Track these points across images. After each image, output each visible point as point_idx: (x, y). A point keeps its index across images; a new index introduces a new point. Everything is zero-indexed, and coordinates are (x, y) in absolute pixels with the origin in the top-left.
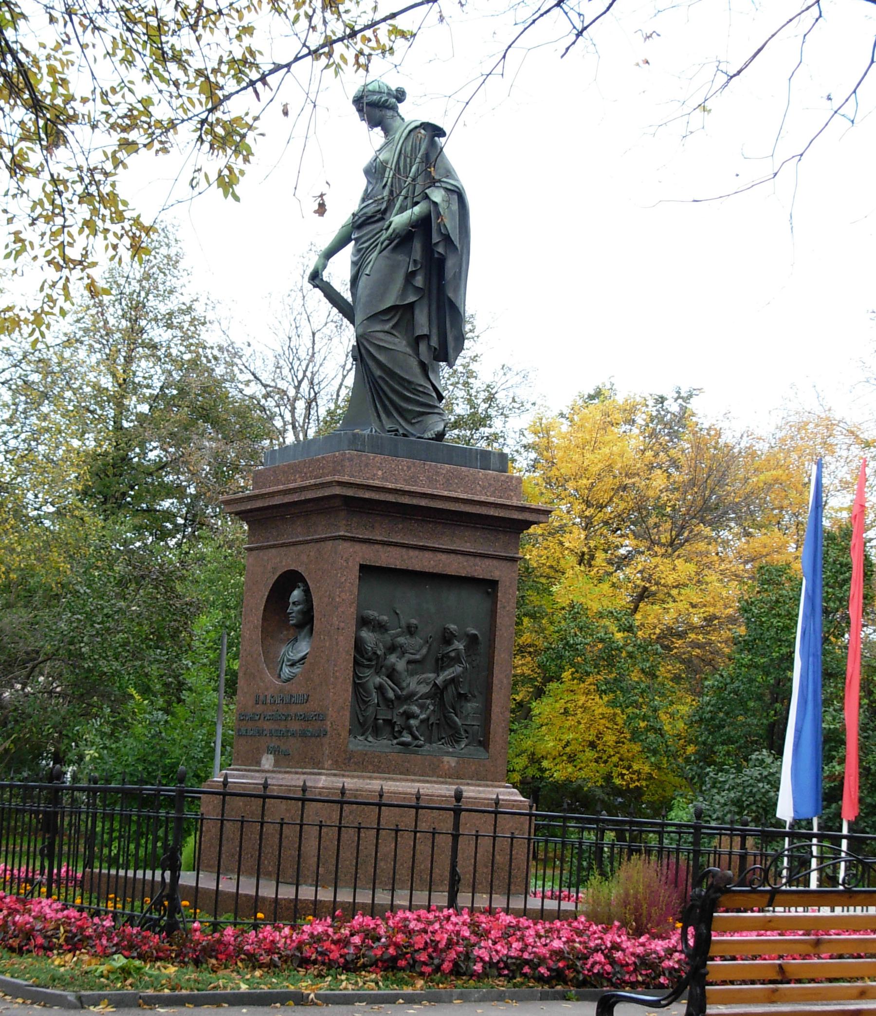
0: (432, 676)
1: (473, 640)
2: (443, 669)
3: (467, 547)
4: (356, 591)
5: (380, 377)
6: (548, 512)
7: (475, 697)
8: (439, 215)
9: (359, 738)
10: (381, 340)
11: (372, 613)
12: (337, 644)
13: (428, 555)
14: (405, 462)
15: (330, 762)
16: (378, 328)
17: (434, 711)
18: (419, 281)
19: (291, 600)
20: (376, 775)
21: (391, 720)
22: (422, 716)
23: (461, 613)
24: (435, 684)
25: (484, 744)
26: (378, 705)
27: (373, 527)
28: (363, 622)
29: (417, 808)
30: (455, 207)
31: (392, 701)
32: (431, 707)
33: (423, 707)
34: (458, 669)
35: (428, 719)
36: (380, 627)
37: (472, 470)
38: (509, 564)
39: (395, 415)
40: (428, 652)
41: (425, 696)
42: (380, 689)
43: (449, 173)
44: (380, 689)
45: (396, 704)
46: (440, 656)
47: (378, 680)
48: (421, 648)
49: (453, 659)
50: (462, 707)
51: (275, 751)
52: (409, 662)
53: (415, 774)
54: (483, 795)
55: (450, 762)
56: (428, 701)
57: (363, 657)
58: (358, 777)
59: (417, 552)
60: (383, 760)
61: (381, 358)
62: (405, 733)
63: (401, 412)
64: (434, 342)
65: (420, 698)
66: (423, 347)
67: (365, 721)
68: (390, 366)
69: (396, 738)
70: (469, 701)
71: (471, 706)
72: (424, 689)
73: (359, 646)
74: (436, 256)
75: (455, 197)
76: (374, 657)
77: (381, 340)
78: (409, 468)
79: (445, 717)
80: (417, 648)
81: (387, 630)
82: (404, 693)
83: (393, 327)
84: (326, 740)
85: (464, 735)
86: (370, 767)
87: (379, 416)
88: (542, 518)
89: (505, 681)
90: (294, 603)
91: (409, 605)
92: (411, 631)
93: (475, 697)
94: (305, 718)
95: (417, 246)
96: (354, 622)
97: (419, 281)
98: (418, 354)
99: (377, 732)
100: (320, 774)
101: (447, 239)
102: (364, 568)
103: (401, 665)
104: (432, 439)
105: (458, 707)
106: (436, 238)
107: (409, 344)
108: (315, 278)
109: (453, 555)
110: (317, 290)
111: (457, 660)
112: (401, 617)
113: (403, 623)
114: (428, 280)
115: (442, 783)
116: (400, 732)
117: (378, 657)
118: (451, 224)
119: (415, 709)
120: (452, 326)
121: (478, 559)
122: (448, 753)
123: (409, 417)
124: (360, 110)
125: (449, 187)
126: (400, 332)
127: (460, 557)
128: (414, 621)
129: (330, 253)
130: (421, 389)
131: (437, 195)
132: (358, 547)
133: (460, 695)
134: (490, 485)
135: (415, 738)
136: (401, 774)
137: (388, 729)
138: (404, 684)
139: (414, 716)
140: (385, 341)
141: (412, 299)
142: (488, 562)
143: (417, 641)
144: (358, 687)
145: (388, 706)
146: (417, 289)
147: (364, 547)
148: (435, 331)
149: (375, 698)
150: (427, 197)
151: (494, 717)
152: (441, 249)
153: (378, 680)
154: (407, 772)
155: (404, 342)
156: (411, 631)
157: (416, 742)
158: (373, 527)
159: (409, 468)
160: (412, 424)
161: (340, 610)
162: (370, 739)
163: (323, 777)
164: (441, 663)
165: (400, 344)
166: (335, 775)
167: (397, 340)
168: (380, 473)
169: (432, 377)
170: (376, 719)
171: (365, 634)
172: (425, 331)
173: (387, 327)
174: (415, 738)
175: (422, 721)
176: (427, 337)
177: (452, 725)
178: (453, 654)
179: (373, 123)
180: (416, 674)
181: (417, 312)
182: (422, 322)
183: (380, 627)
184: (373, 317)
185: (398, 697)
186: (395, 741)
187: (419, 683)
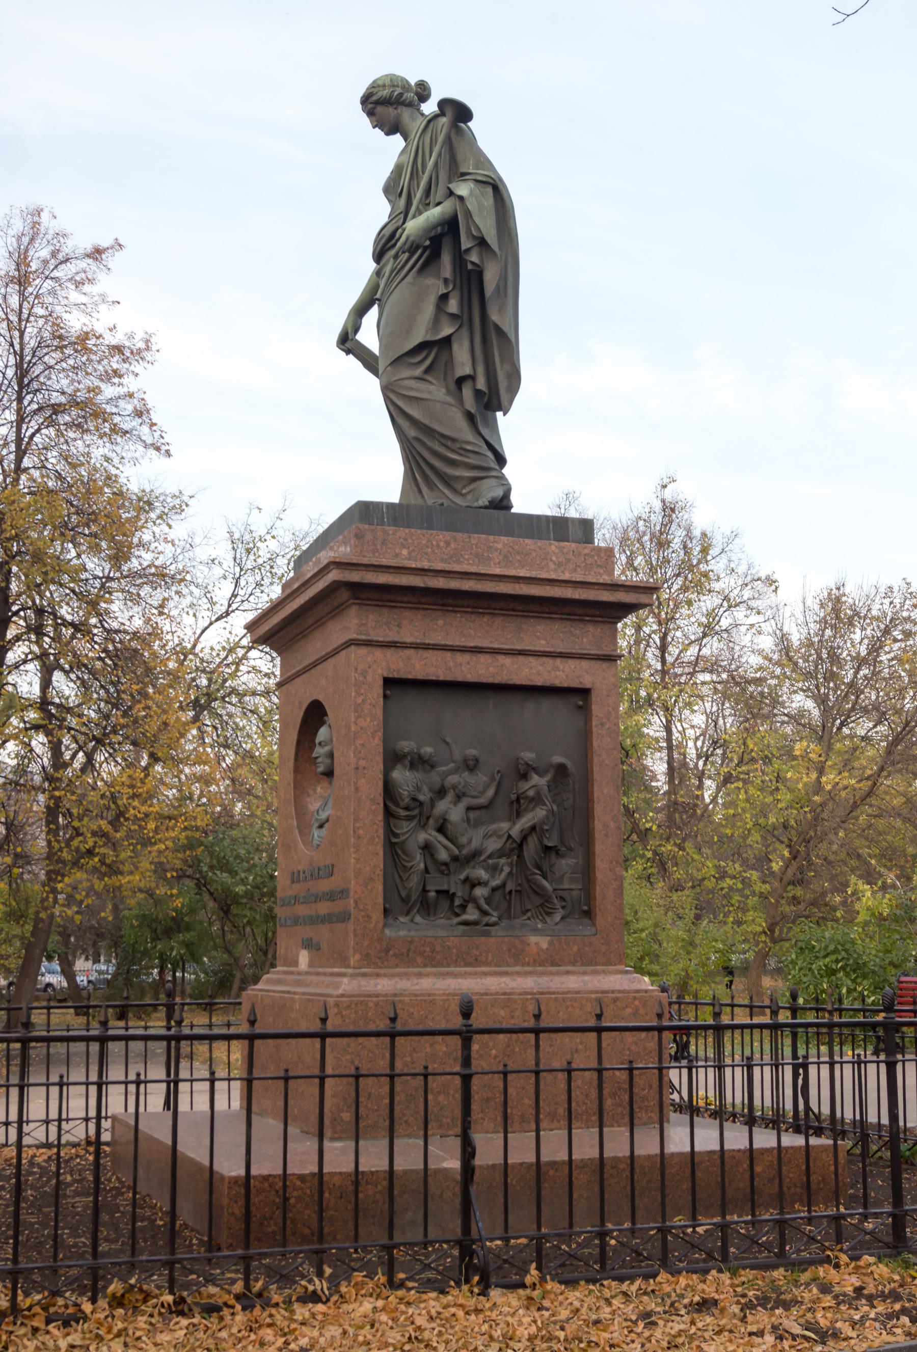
0: (505, 825)
1: (561, 769)
2: (519, 815)
3: (542, 645)
4: (380, 714)
5: (417, 439)
6: (652, 589)
7: (571, 850)
8: (468, 214)
9: (402, 919)
10: (411, 389)
11: (406, 745)
12: (357, 789)
13: (483, 658)
14: (441, 536)
15: (357, 957)
16: (407, 373)
17: (510, 873)
18: (453, 306)
19: (317, 741)
20: (429, 970)
21: (447, 892)
22: (496, 882)
23: (539, 734)
24: (510, 837)
25: (588, 914)
26: (426, 870)
27: (399, 626)
28: (393, 758)
29: (393, 1035)
30: (489, 200)
31: (446, 864)
32: (507, 869)
33: (494, 870)
34: (540, 813)
35: (503, 885)
36: (418, 762)
37: (540, 543)
38: (605, 665)
39: (441, 487)
40: (497, 792)
41: (500, 853)
42: (427, 848)
43: (483, 161)
44: (427, 848)
45: (452, 867)
46: (514, 797)
47: (422, 837)
48: (487, 787)
49: (532, 799)
50: (552, 866)
51: (308, 944)
52: (469, 809)
53: (488, 964)
54: (590, 987)
55: (539, 942)
56: (503, 861)
57: (398, 805)
58: (400, 975)
59: (467, 657)
60: (438, 948)
61: (414, 413)
62: (470, 908)
63: (447, 481)
64: (481, 384)
65: (490, 857)
66: (467, 392)
67: (409, 896)
68: (426, 421)
69: (457, 915)
70: (563, 856)
71: (566, 864)
72: (493, 845)
73: (389, 791)
74: (470, 267)
75: (490, 190)
76: (413, 805)
77: (411, 389)
78: (448, 543)
79: (528, 881)
80: (481, 788)
81: (433, 767)
82: (464, 852)
83: (428, 371)
84: (351, 926)
85: (558, 904)
86: (419, 960)
87: (420, 491)
88: (643, 599)
89: (612, 825)
90: (320, 744)
91: (463, 730)
92: (471, 765)
93: (571, 850)
94: (331, 897)
95: (446, 260)
96: (380, 758)
97: (453, 306)
98: (461, 402)
99: (426, 907)
100: (343, 975)
101: (482, 243)
102: (390, 683)
103: (456, 814)
104: (486, 507)
105: (546, 867)
106: (465, 243)
107: (449, 392)
108: (347, 341)
109: (521, 658)
110: (351, 356)
111: (537, 800)
112: (454, 746)
113: (457, 756)
114: (466, 303)
115: (530, 973)
116: (463, 907)
117: (421, 804)
118: (487, 227)
119: (482, 874)
120: (502, 361)
121: (558, 661)
122: (535, 931)
123: (458, 486)
124: (370, 114)
125: (480, 178)
126: (436, 378)
127: (531, 659)
128: (472, 752)
129: (360, 310)
130: (469, 447)
131: (463, 189)
132: (378, 653)
133: (548, 849)
134: (568, 561)
135: (484, 913)
136: (467, 964)
137: (445, 904)
138: (463, 840)
139: (479, 883)
140: (416, 390)
141: (447, 331)
142: (572, 663)
143: (478, 780)
144: (394, 849)
145: (442, 872)
146: (453, 316)
147: (389, 653)
148: (480, 370)
149: (419, 862)
150: (451, 193)
151: (599, 875)
152: (474, 258)
153: (422, 837)
154: (477, 962)
155: (444, 390)
156: (471, 765)
157: (486, 919)
158: (399, 626)
159: (448, 543)
160: (462, 495)
161: (359, 742)
162: (418, 919)
163: (345, 980)
164: (518, 806)
165: (436, 391)
166: (364, 975)
167: (431, 387)
168: (405, 552)
169: (484, 431)
170: (425, 891)
171: (400, 775)
172: (467, 370)
173: (418, 372)
174: (484, 913)
175: (494, 890)
176: (472, 378)
177: (539, 892)
178: (531, 793)
179: (391, 128)
180: (482, 824)
181: (455, 347)
182: (462, 358)
183: (418, 762)
184: (397, 361)
185: (455, 859)
186: (456, 920)
187: (486, 837)
